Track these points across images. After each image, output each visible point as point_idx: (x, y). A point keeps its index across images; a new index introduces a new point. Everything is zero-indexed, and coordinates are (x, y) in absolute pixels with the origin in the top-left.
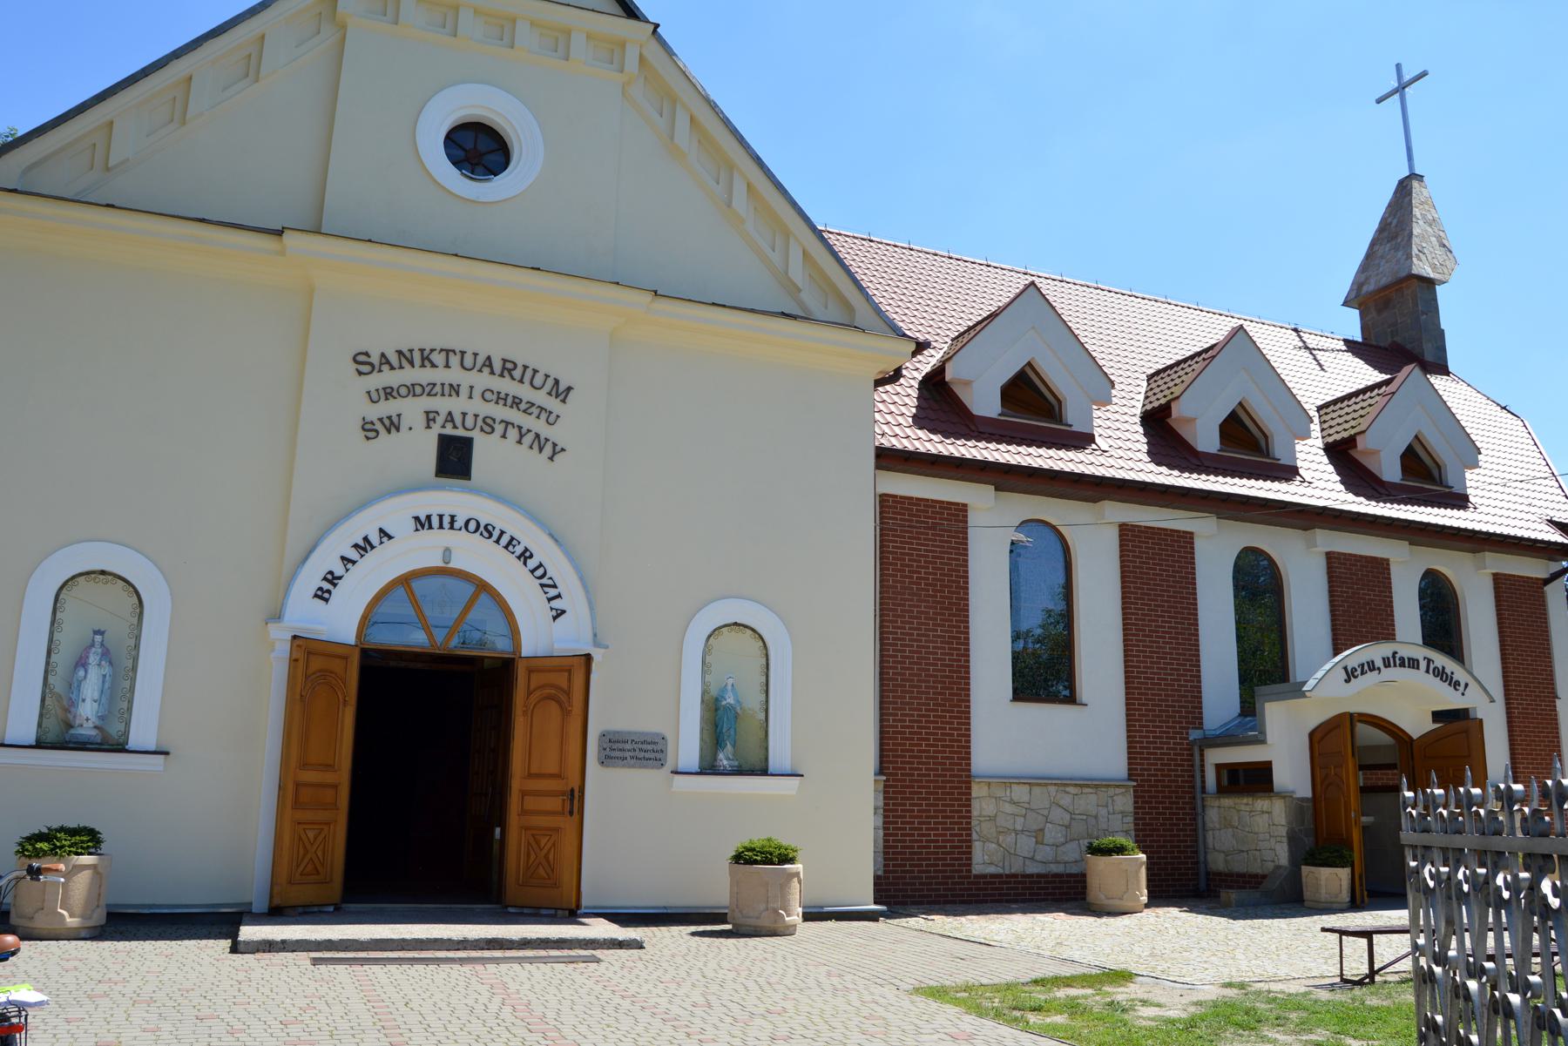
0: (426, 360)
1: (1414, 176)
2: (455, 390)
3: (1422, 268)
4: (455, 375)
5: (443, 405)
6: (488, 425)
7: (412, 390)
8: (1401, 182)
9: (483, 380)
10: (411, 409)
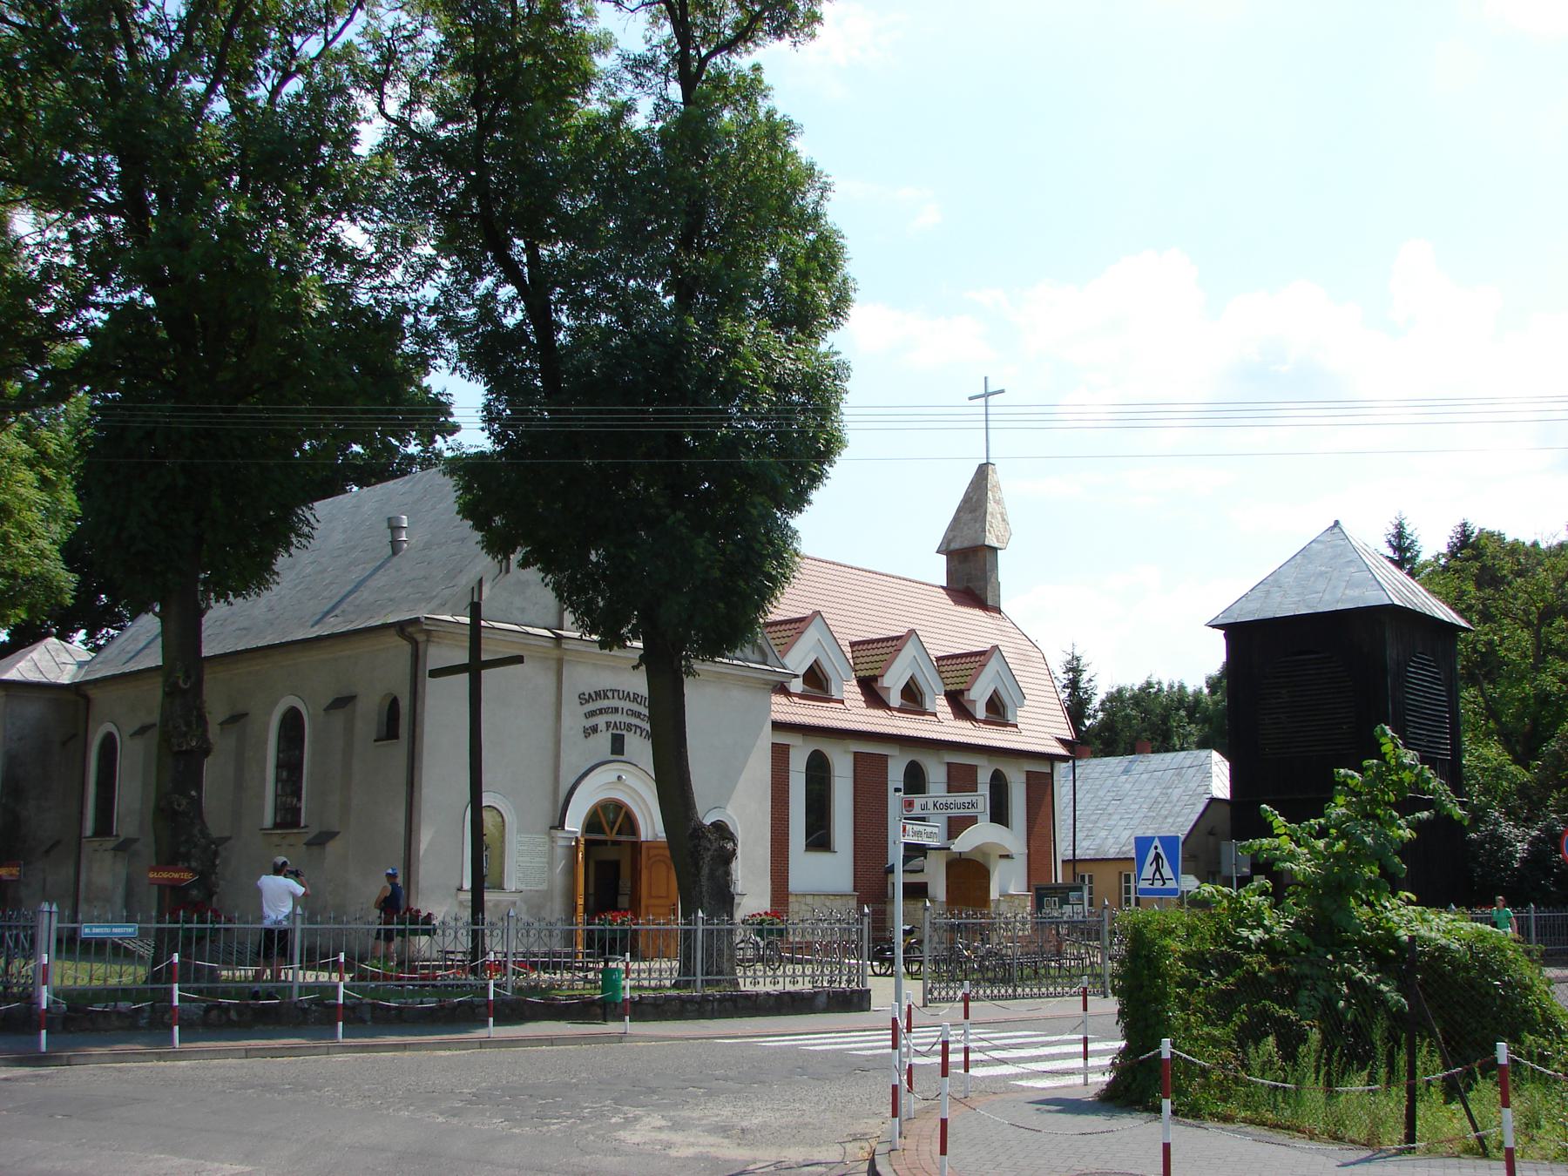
0: (606, 697)
1: (987, 464)
2: (616, 710)
3: (991, 540)
4: (615, 703)
5: (613, 718)
6: (629, 727)
7: (601, 711)
8: (981, 466)
9: (627, 705)
10: (600, 721)
